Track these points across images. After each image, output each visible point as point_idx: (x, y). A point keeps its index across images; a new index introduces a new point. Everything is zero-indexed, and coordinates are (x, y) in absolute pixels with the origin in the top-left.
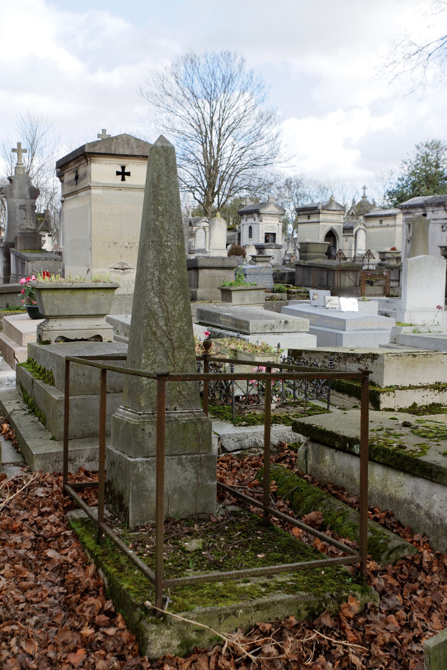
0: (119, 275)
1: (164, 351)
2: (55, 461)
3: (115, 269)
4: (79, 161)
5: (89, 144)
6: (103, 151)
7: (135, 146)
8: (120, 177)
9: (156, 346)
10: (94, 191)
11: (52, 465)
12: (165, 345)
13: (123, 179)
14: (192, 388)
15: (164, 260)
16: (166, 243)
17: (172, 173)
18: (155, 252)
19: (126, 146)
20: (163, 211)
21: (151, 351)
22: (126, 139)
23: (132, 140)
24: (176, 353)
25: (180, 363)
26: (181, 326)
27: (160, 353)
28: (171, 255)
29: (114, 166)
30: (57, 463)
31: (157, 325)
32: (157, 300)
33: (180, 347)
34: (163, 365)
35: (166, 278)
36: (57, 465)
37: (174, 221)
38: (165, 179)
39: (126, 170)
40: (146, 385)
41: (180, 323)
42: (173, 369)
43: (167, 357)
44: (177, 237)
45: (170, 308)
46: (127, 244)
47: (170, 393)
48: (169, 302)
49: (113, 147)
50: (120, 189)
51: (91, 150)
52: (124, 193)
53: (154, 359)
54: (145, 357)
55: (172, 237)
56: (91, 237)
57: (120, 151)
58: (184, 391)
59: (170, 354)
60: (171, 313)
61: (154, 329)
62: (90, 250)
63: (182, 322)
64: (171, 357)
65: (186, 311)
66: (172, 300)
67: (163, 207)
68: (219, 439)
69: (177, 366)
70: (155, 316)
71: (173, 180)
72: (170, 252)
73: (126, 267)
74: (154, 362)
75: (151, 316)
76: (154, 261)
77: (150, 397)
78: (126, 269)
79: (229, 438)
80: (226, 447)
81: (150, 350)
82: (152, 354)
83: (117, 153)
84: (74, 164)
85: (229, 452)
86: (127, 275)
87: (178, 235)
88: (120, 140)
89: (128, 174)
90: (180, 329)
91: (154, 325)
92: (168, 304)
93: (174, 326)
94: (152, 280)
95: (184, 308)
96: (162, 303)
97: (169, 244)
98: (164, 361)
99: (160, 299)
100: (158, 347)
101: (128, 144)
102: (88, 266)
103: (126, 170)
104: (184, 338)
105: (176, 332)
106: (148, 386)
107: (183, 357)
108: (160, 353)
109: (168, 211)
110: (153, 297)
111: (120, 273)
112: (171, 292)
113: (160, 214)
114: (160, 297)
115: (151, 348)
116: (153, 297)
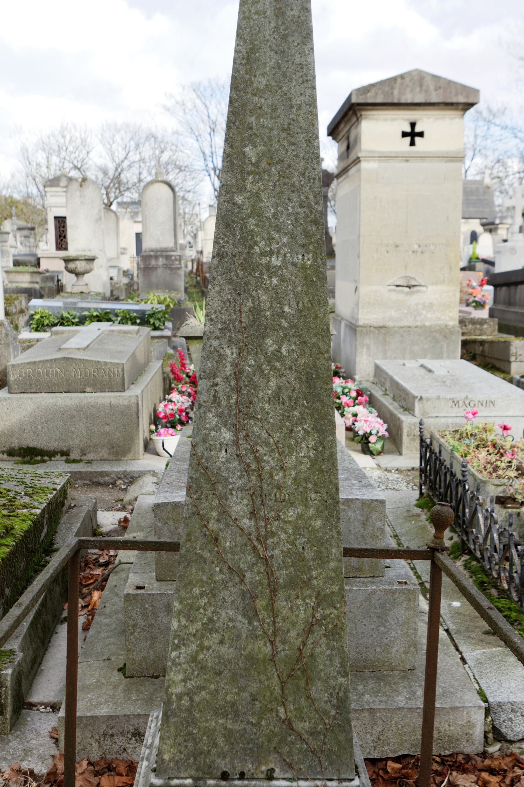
0: (401, 297)
1: (243, 594)
2: (105, 735)
3: (397, 286)
4: (349, 120)
5: (358, 90)
6: (379, 100)
7: (432, 87)
8: (408, 139)
9: (218, 577)
10: (364, 165)
11: (98, 741)
12: (248, 575)
13: (412, 143)
14: (326, 713)
15: (257, 312)
16: (264, 260)
17: (295, 39)
18: (227, 288)
19: (418, 89)
20: (259, 161)
21: (202, 594)
22: (419, 78)
23: (428, 79)
24: (281, 603)
25: (293, 634)
26: (300, 517)
27: (229, 599)
28: (278, 297)
29: (400, 121)
30: (108, 738)
31: (224, 512)
32: (227, 435)
33: (292, 583)
34: (239, 637)
35: (259, 368)
36: (109, 742)
37: (295, 189)
38: (269, 58)
39: (417, 129)
40: (180, 697)
41: (300, 509)
42: (268, 650)
43: (251, 614)
44: (301, 240)
45: (270, 462)
46: (416, 247)
47: (257, 725)
48: (267, 444)
49: (396, 92)
50: (407, 158)
51: (361, 100)
52: (413, 165)
53: (211, 620)
54: (180, 612)
55: (285, 240)
56: (359, 237)
57: (408, 98)
58: (302, 719)
59: (261, 603)
60: (271, 476)
61: (213, 525)
62: (359, 257)
63: (307, 507)
64: (263, 614)
65: (321, 471)
66: (277, 435)
67: (261, 148)
68: (488, 711)
69: (284, 642)
70: (220, 487)
71: (298, 60)
72: (275, 289)
73: (414, 283)
74: (210, 627)
75: (206, 487)
76: (225, 317)
77: (190, 734)
78: (414, 286)
79: (513, 711)
80: (504, 730)
81: (197, 591)
82: (203, 601)
83: (403, 101)
84: (345, 126)
85: (511, 742)
86: (415, 296)
87: (306, 234)
88: (407, 79)
89: (421, 134)
90: (297, 529)
91: (214, 514)
92: (262, 450)
93: (277, 518)
94: (214, 376)
95: (314, 462)
96: (244, 445)
97: (275, 261)
98: (242, 624)
99: (236, 434)
100: (225, 583)
101: (421, 86)
102: (356, 281)
103: (417, 129)
104: (309, 555)
105: (283, 536)
106: (185, 702)
107: (302, 615)
108: (229, 599)
109: (276, 159)
110: (216, 428)
111: (402, 292)
112: (273, 412)
113: (250, 168)
114: (236, 429)
115: (202, 583)
116: (216, 428)
